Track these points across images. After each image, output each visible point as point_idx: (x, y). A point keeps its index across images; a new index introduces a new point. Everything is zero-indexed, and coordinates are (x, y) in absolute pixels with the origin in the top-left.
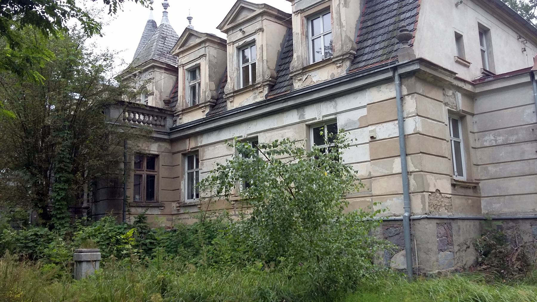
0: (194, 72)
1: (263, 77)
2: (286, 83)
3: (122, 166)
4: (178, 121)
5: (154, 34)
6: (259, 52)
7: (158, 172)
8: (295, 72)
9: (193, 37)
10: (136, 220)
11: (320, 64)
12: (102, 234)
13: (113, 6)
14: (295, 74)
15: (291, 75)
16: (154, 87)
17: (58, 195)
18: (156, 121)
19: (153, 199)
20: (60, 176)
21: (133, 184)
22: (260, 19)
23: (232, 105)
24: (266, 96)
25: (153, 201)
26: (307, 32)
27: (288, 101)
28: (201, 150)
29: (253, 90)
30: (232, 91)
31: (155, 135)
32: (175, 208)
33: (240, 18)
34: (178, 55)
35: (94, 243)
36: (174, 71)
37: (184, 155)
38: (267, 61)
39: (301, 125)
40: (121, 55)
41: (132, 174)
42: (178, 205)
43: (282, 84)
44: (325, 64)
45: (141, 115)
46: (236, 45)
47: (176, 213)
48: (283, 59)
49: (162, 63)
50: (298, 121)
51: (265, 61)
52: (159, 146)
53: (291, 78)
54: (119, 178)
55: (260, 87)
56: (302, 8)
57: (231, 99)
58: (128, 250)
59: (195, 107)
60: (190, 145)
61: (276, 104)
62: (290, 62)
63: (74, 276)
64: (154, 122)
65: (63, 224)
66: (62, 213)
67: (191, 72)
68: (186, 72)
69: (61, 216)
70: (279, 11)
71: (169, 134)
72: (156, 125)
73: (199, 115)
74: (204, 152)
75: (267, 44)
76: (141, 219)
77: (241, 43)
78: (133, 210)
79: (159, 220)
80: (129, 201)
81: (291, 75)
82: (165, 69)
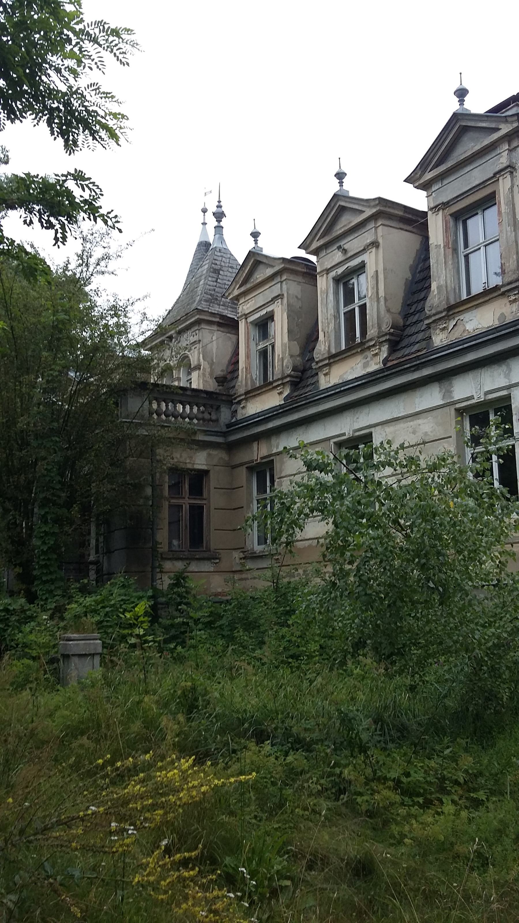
0: (263, 325)
1: (379, 327)
2: (420, 336)
3: (149, 491)
4: (240, 411)
5: (201, 266)
6: (371, 282)
7: (208, 499)
8: (434, 315)
9: (261, 267)
10: (172, 582)
11: (479, 299)
12: (108, 609)
13: (60, 231)
14: (433, 318)
15: (427, 322)
16: (201, 356)
17: (44, 543)
18: (203, 412)
19: (202, 546)
20: (47, 513)
21: (166, 522)
22: (372, 225)
23: (328, 380)
24: (385, 361)
25: (201, 549)
26: (456, 241)
27: (422, 368)
28: (276, 459)
29: (363, 351)
30: (326, 355)
31: (201, 437)
32: (237, 560)
33: (338, 227)
34: (237, 298)
35: (92, 623)
36: (230, 325)
37: (251, 469)
38: (386, 299)
39: (447, 409)
40: (139, 307)
41: (166, 504)
42: (242, 555)
43: (413, 339)
44: (487, 298)
45: (170, 404)
46: (333, 274)
47: (239, 568)
48: (414, 293)
49: (213, 314)
50: (441, 402)
51: (382, 302)
52: (209, 455)
53: (429, 326)
54: (145, 512)
55: (374, 346)
56: (445, 201)
57: (326, 370)
58: (138, 636)
59: (267, 385)
60: (260, 451)
61: (402, 375)
62: (425, 298)
63: (59, 679)
64: (200, 416)
65: (51, 591)
66: (51, 573)
67: (259, 327)
68: (250, 327)
69: (49, 577)
70: (405, 207)
71: (224, 434)
72: (204, 419)
73: (273, 400)
74: (282, 463)
75: (385, 269)
76: (179, 579)
77: (340, 270)
78: (168, 565)
79: (208, 581)
80: (160, 550)
81: (427, 322)
82: (219, 324)
